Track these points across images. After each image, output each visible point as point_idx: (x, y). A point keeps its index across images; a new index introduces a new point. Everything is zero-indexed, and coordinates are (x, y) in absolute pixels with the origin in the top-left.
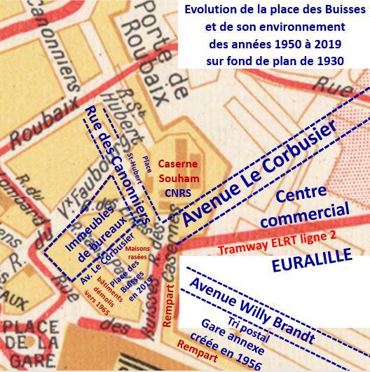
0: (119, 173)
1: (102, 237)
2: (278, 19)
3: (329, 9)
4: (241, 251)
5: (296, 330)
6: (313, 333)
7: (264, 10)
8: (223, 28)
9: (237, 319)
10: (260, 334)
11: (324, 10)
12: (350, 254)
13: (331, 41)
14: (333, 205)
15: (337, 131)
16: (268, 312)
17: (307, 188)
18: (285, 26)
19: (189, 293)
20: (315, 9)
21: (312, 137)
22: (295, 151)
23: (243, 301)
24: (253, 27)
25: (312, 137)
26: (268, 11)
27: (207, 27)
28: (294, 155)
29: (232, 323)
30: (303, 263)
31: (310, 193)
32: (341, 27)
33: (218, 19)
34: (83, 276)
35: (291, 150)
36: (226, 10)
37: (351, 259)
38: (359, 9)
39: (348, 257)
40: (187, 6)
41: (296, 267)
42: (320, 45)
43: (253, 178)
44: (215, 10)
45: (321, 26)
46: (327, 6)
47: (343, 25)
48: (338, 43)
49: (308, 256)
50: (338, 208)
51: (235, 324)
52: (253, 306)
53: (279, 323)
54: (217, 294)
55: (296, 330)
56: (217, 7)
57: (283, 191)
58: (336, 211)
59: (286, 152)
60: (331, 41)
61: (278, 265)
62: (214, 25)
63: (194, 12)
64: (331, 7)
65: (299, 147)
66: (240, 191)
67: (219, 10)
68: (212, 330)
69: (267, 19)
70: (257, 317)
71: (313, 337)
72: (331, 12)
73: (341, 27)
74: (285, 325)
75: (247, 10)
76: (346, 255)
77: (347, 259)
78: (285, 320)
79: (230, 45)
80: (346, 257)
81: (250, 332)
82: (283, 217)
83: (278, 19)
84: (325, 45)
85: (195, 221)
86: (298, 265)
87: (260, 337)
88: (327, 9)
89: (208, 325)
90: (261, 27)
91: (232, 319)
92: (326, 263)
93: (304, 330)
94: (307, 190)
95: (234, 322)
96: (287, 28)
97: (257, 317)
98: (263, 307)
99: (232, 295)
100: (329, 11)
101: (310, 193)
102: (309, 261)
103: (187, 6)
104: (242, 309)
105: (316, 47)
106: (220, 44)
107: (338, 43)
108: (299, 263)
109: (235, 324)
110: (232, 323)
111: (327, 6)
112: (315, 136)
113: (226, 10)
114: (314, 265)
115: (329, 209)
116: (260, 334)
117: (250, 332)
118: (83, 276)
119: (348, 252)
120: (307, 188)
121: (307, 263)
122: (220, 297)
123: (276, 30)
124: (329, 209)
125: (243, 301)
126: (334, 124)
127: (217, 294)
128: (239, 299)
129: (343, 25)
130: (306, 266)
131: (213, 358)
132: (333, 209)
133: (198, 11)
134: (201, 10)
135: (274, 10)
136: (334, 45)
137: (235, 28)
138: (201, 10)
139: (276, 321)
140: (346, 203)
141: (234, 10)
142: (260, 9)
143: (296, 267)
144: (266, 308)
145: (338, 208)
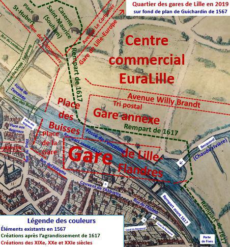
5: (190, 103)
6: (199, 102)
14: (171, 55)
15: (48, 14)
16: (173, 99)
17: (152, 36)
23: (158, 98)
31: (155, 42)
34: (10, 40)
42: (218, 5)
51: (119, 105)
53: (180, 102)
55: (190, 103)
57: (132, 36)
66: (167, 44)
74: (183, 102)
79: (24, 229)
81: (129, 106)
87: (136, 107)
91: (115, 102)
94: (152, 38)
95: (118, 103)
98: (169, 97)
99: (151, 96)
101: (155, 42)
104: (158, 101)
109: (119, 105)
115: (168, 58)
116: (135, 105)
117: (129, 106)
118: (10, 40)
120: (152, 36)
124: (168, 58)
125: (158, 98)
128: (155, 97)
132: (171, 58)
140: (183, 55)
144: (171, 97)
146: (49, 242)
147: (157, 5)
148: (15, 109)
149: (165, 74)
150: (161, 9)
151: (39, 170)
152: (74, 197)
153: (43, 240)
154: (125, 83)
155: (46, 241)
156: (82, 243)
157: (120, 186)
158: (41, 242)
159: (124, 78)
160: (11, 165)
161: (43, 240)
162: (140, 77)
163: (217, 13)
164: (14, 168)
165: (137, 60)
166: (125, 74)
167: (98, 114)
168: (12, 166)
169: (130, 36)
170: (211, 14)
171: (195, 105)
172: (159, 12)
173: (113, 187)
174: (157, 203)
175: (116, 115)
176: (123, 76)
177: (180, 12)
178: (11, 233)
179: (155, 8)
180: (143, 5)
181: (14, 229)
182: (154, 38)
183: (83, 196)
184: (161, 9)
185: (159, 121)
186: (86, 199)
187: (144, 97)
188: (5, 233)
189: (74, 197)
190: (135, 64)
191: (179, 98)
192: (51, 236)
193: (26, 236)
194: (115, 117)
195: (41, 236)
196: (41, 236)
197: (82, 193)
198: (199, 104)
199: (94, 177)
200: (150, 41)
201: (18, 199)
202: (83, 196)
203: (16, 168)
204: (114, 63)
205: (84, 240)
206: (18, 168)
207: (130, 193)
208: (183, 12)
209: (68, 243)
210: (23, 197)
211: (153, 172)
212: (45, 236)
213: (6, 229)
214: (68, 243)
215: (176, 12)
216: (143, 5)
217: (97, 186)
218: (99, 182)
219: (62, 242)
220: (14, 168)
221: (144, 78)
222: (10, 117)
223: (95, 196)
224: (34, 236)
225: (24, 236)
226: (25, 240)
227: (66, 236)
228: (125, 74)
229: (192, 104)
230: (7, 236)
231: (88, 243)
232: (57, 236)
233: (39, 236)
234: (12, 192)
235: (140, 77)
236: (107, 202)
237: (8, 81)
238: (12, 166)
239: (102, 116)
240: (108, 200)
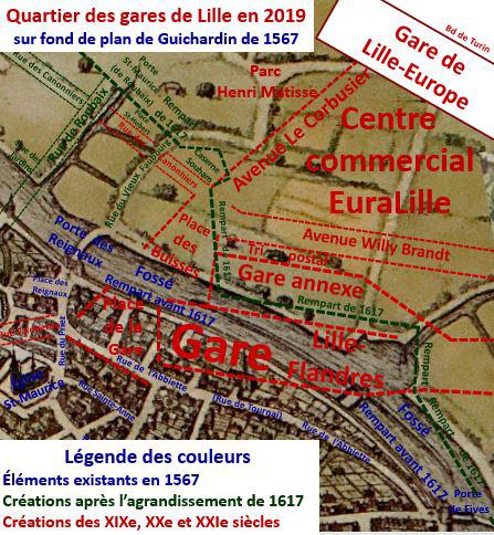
6: (446, 248)
13: (290, 11)
17: (400, 110)
19: (464, 392)
20: (161, 457)
28: (333, 108)
35: (329, 103)
42: (273, 18)
48: (301, 13)
50: (453, 157)
58: (449, 161)
60: (290, 11)
61: (341, 202)
67: (56, 17)
68: (462, 169)
71: (447, 253)
74: (414, 249)
78: (414, 244)
84: (279, 17)
85: (245, 184)
89: (406, 36)
92: (373, 56)
93: (437, 248)
97: (378, 59)
100: (406, 251)
105: (267, 20)
106: (102, 15)
107: (301, 13)
112: (351, 86)
115: (437, 157)
120: (400, 110)
124: (437, 157)
126: (78, 16)
136: (295, 17)
139: (404, 249)
145: (453, 157)
146: (150, 522)
147: (81, 18)
148: (38, 249)
149: (430, 192)
150: (98, 30)
151: (89, 369)
152: (166, 418)
153: (131, 513)
154: (342, 212)
155: (140, 516)
156: (247, 523)
157: (268, 396)
158: (124, 522)
160: (29, 358)
161: (131, 513)
162: (374, 199)
164: (33, 366)
165: (367, 159)
166: (341, 193)
167: (402, 37)
168: (30, 362)
169: (351, 109)
170: (145, 48)
171: (439, 255)
172: (92, 40)
173: (253, 398)
174: (352, 430)
175: (433, 50)
176: (338, 197)
177: (156, 40)
178: (32, 491)
179: (79, 27)
180: (37, 17)
181: (42, 481)
182: (404, 114)
183: (187, 416)
184: (98, 30)
185: (301, 130)
186: (194, 422)
188: (16, 491)
189: (166, 418)
190: (363, 169)
191: (408, 242)
192: (154, 503)
193: (80, 502)
195: (125, 502)
196: (125, 502)
197: (183, 411)
198: (447, 253)
199: (210, 378)
201: (42, 424)
202: (187, 416)
203: (38, 365)
205: (255, 513)
206: (41, 365)
207: (292, 410)
208: (164, 39)
209: (205, 522)
210: (53, 420)
211: (362, 379)
212: (138, 504)
213: (19, 482)
214: (205, 522)
215: (142, 39)
216: (37, 17)
217: (131, 368)
218: (222, 389)
219: (189, 520)
220: (33, 366)
221: (384, 202)
222: (26, 264)
223: (213, 416)
224: (103, 502)
225: (73, 502)
226: (74, 513)
227: (199, 502)
228: (341, 193)
230: (22, 502)
231: (268, 524)
232: (174, 501)
233: (117, 502)
234: (31, 411)
235: (374, 199)
236: (239, 428)
237: (308, 234)
238: (30, 362)
240: (243, 424)
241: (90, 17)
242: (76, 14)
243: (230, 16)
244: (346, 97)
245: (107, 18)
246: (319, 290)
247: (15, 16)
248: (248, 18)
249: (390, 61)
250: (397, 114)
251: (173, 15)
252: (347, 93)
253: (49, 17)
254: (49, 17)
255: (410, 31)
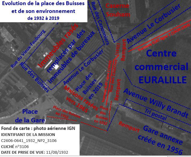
0: (177, 113)
1: (83, 43)
2: (44, 8)
3: (68, 3)
4: (150, 69)
5: (179, 112)
7: (38, 4)
8: (20, 12)
9: (149, 110)
10: (161, 116)
11: (65, 3)
12: (185, 80)
17: (165, 51)
18: (48, 11)
21: (172, 12)
22: (166, 15)
24: (33, 11)
25: (172, 12)
26: (40, 4)
27: (12, 11)
29: (147, 111)
30: (157, 81)
31: (167, 54)
32: (73, 11)
33: (18, 7)
35: (164, 15)
36: (21, 4)
37: (186, 83)
38: (81, 3)
39: (185, 81)
40: (3, 2)
41: (153, 83)
42: (51, 19)
43: (151, 25)
44: (16, 3)
45: (64, 11)
46: (67, 2)
47: (74, 10)
49: (161, 77)
51: (149, 112)
52: (156, 101)
54: (138, 96)
56: (17, 3)
59: (163, 16)
62: (16, 10)
63: (6, 5)
64: (68, 2)
65: (50, 56)
67: (18, 4)
69: (39, 8)
70: (158, 106)
72: (69, 4)
73: (73, 11)
75: (30, 4)
76: (183, 80)
77: (183, 82)
80: (183, 81)
82: (55, 75)
83: (44, 8)
86: (154, 81)
87: (162, 118)
88: (67, 3)
89: (147, 129)
90: (37, 11)
91: (147, 109)
92: (170, 83)
95: (148, 111)
96: (48, 11)
101: (167, 54)
102: (161, 80)
103: (3, 2)
105: (50, 19)
108: (155, 80)
109: (149, 112)
110: (147, 111)
111: (67, 2)
112: (173, 10)
113: (21, 4)
114: (163, 83)
116: (161, 116)
119: (184, 78)
120: (165, 51)
121: (159, 81)
122: (140, 96)
123: (44, 12)
126: (180, 5)
127: (138, 96)
129: (74, 10)
130: (158, 83)
131: (137, 130)
133: (8, 4)
134: (9, 4)
135: (43, 4)
136: (56, 19)
137: (25, 12)
138: (9, 4)
141: (24, 4)
142: (37, 3)
143: (153, 83)
154: (143, 83)
159: (142, 80)
163: (35, 19)
167: (146, 129)
182: (166, 52)
185: (155, 143)
187: (140, 99)
194: (156, 134)
200: (164, 53)
204: (138, 69)
229: (181, 112)
239: (148, 131)
241: (14, 129)
242: (179, 5)
243: (24, 11)
244: (171, 13)
245: (82, 4)
246: (156, 69)
247: (55, 141)
248: (39, 12)
249: (67, 62)
250: (164, 52)
251: (97, 12)
252: (171, 12)
253: (25, 129)
254: (25, 129)
255: (148, 127)
